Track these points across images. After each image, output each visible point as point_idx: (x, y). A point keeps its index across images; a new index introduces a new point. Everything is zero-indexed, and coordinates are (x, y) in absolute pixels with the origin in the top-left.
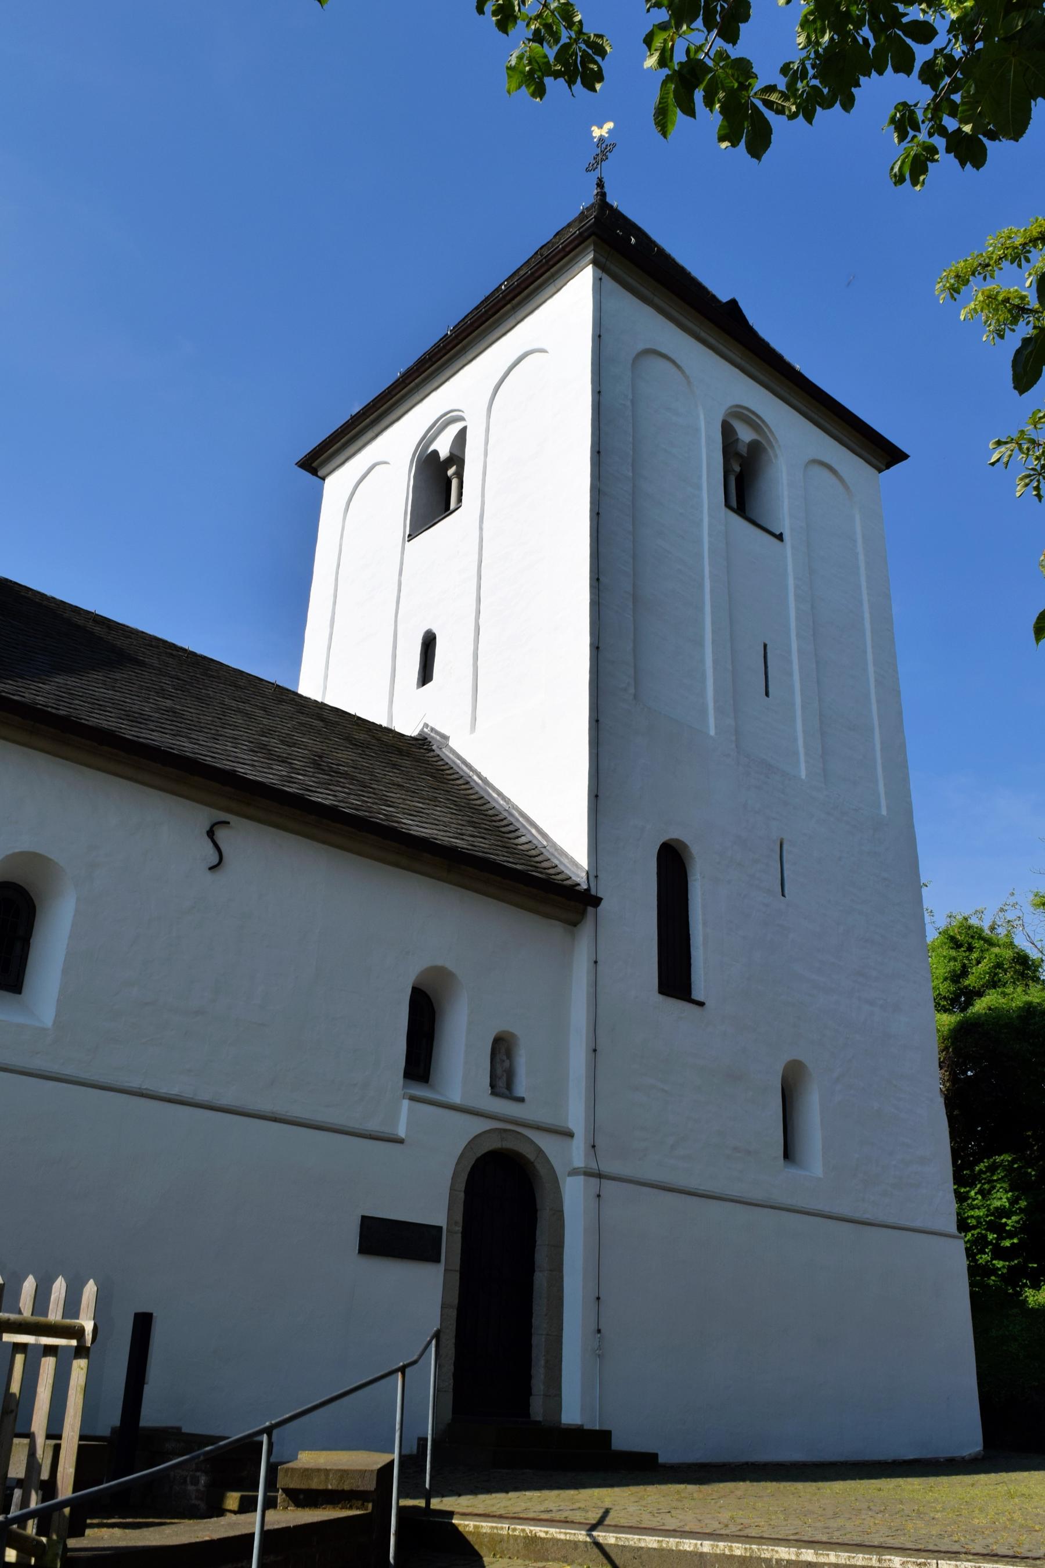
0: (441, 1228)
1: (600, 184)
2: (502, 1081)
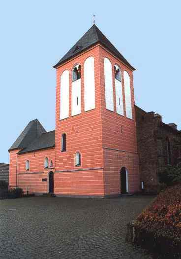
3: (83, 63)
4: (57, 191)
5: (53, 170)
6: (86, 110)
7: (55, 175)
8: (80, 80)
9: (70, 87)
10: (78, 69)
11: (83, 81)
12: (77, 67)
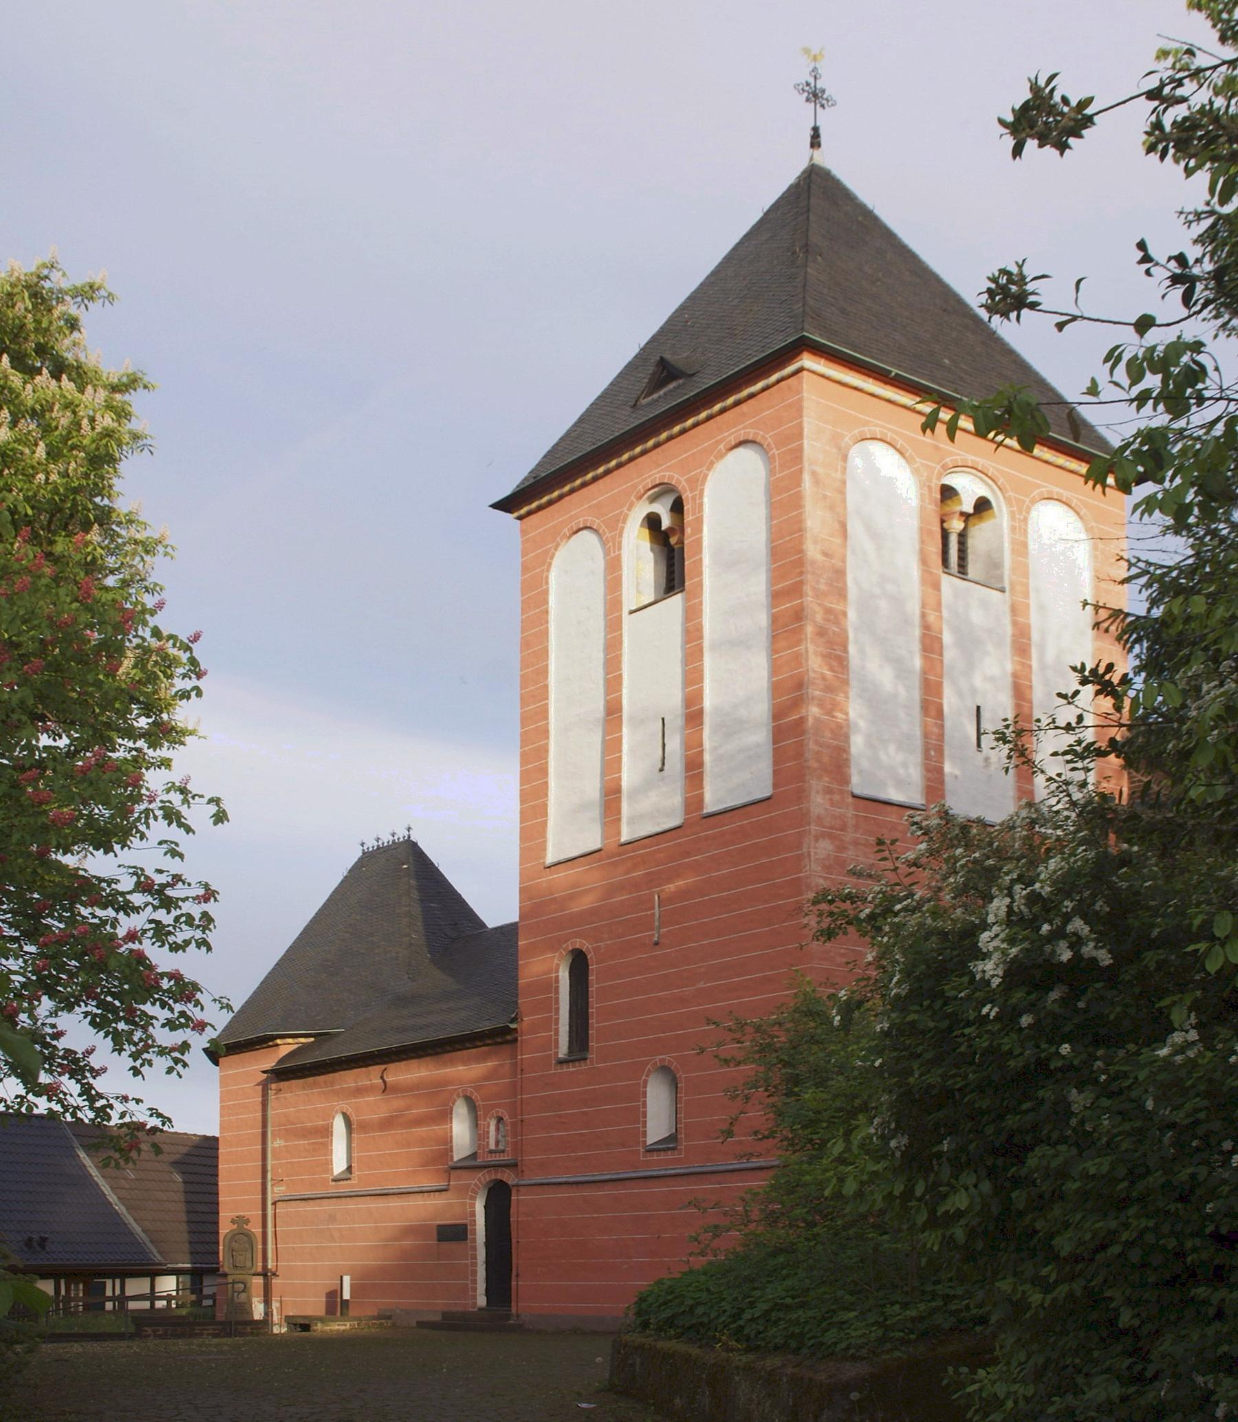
3: (698, 483)
4: (534, 1296)
5: (509, 1178)
6: (711, 805)
8: (677, 600)
9: (613, 648)
10: (666, 523)
11: (692, 616)
12: (663, 510)
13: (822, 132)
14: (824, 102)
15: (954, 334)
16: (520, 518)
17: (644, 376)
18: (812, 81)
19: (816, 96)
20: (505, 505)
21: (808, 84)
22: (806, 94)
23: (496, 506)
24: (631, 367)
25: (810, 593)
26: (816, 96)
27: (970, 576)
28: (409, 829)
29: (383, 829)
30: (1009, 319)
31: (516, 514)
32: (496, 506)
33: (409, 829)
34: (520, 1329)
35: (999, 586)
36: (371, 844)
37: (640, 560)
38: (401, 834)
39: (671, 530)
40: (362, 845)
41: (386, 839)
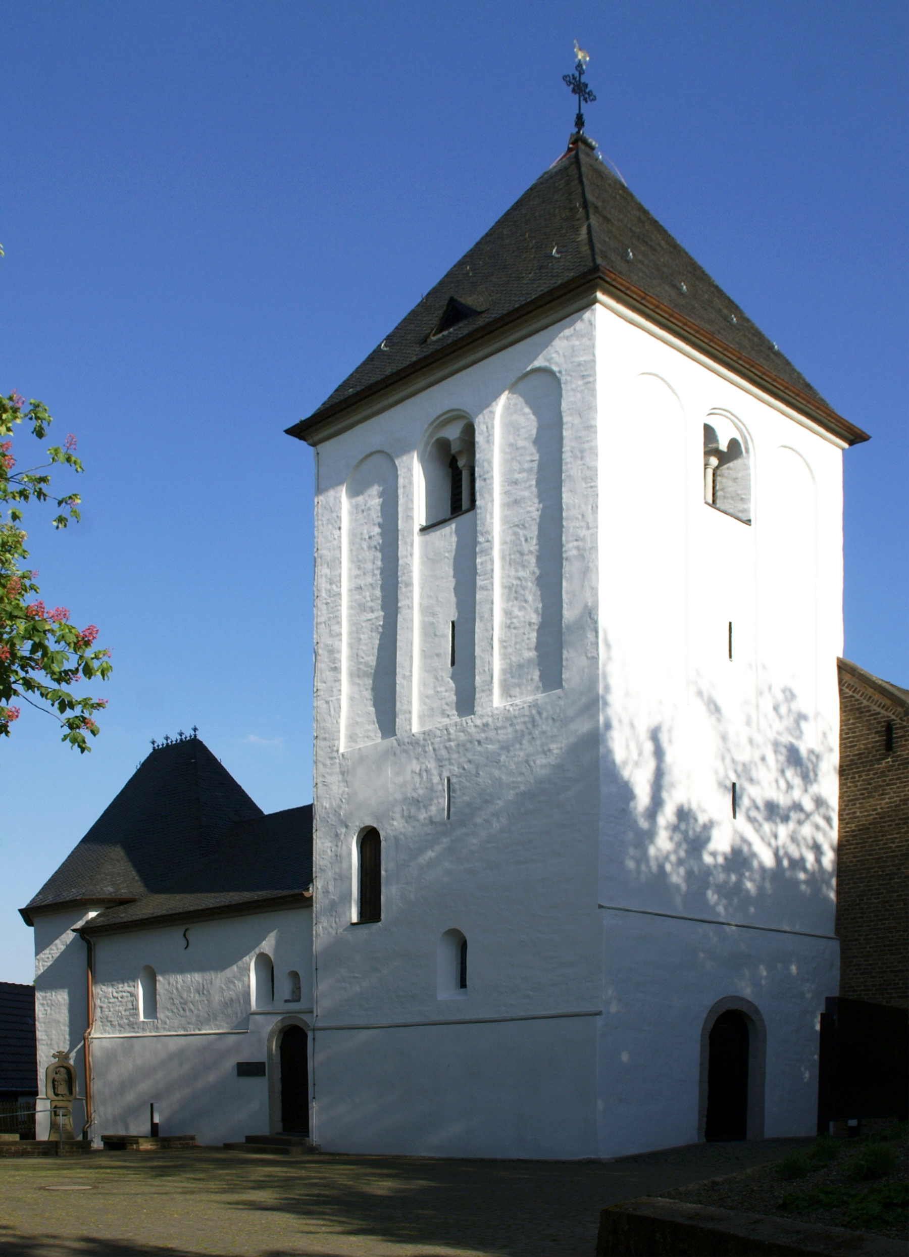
0: (264, 1063)
1: (580, 122)
2: (296, 997)
7: (319, 1057)
13: (585, 117)
14: (586, 96)
15: (706, 296)
16: (314, 445)
17: (434, 319)
18: (577, 74)
19: (580, 89)
20: (300, 431)
21: (574, 78)
22: (572, 86)
23: (291, 432)
24: (413, 317)
25: (530, 598)
26: (580, 89)
27: (718, 506)
28: (195, 730)
29: (169, 730)
30: (15, 692)
31: (311, 441)
32: (291, 432)
33: (195, 730)
34: (312, 1150)
35: (745, 519)
36: (161, 742)
37: (416, 481)
38: (188, 733)
39: (460, 452)
40: (153, 743)
41: (174, 737)
